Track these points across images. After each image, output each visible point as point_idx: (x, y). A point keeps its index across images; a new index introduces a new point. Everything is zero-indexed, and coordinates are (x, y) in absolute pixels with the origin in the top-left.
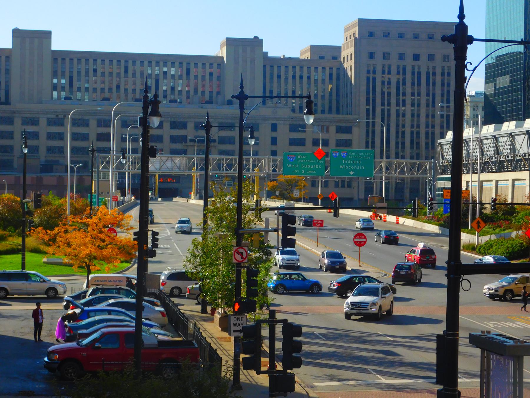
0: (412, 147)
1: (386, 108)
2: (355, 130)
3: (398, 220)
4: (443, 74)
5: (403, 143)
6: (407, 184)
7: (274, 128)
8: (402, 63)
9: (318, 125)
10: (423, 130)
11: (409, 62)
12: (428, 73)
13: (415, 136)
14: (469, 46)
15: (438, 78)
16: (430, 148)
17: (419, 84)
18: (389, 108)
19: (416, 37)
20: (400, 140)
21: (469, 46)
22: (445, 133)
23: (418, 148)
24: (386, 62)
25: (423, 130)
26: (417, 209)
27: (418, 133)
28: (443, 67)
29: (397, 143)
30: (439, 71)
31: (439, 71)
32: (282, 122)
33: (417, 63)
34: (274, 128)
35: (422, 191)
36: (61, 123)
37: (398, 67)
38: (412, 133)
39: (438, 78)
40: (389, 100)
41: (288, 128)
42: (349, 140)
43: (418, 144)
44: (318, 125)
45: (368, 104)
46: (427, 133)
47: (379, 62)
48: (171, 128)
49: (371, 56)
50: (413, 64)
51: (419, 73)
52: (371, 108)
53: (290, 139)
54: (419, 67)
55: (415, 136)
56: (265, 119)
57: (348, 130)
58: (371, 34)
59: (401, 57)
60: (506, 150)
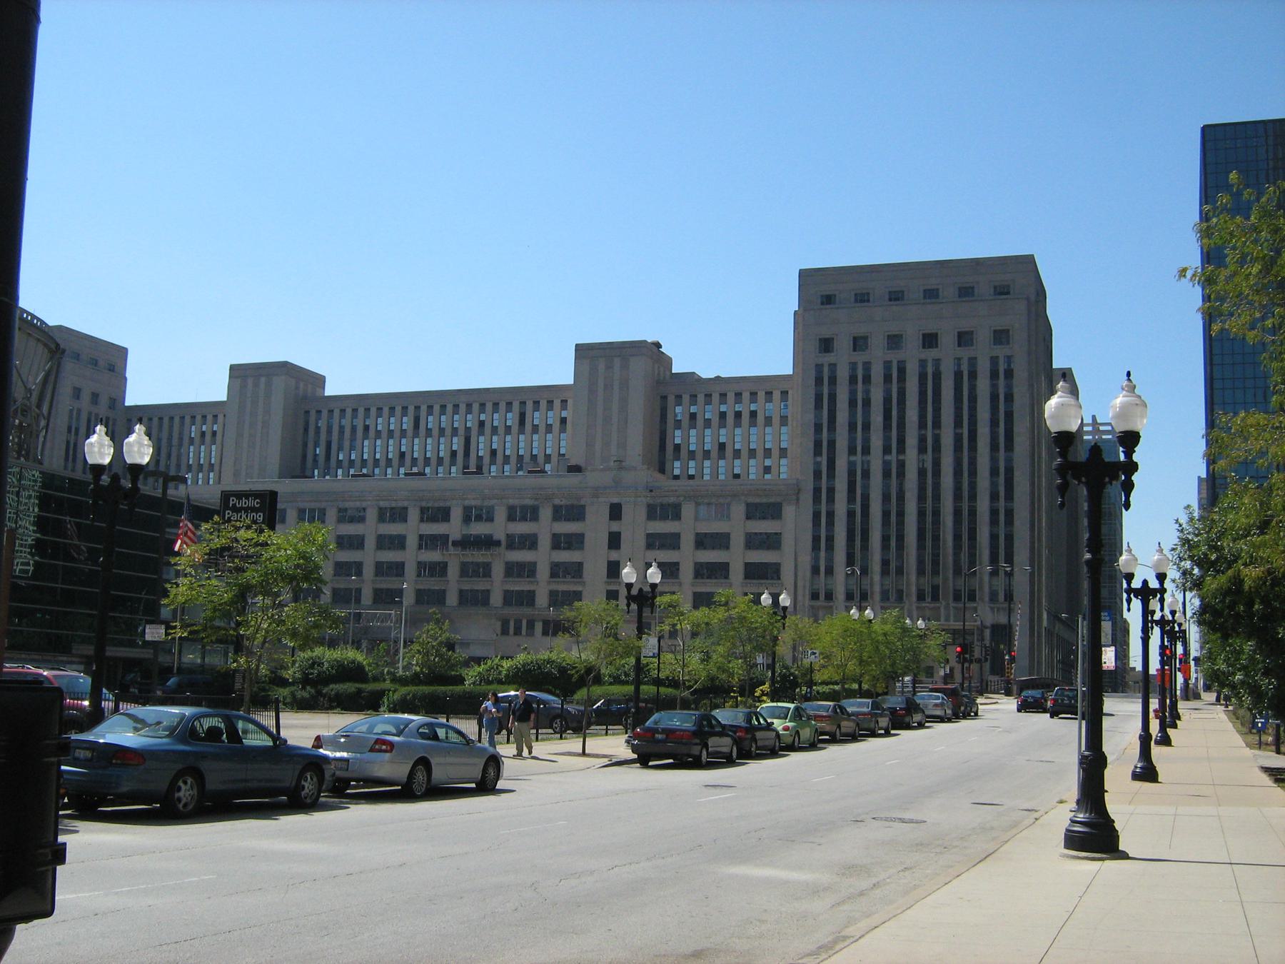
1: (893, 457)
2: (789, 511)
3: (165, 488)
4: (994, 375)
7: (616, 512)
8: (894, 357)
9: (709, 504)
11: (912, 354)
12: (958, 375)
14: (676, 369)
15: (983, 385)
17: (994, 398)
18: (853, 458)
19: (931, 294)
21: (676, 369)
24: (965, 353)
28: (959, 359)
30: (984, 367)
31: (984, 367)
33: (931, 354)
34: (616, 512)
36: (421, 596)
37: (887, 365)
39: (983, 385)
40: (866, 441)
41: (643, 512)
44: (709, 504)
47: (843, 357)
48: (422, 520)
50: (923, 357)
51: (937, 376)
54: (937, 362)
56: (597, 492)
57: (773, 511)
58: (828, 300)
59: (894, 341)
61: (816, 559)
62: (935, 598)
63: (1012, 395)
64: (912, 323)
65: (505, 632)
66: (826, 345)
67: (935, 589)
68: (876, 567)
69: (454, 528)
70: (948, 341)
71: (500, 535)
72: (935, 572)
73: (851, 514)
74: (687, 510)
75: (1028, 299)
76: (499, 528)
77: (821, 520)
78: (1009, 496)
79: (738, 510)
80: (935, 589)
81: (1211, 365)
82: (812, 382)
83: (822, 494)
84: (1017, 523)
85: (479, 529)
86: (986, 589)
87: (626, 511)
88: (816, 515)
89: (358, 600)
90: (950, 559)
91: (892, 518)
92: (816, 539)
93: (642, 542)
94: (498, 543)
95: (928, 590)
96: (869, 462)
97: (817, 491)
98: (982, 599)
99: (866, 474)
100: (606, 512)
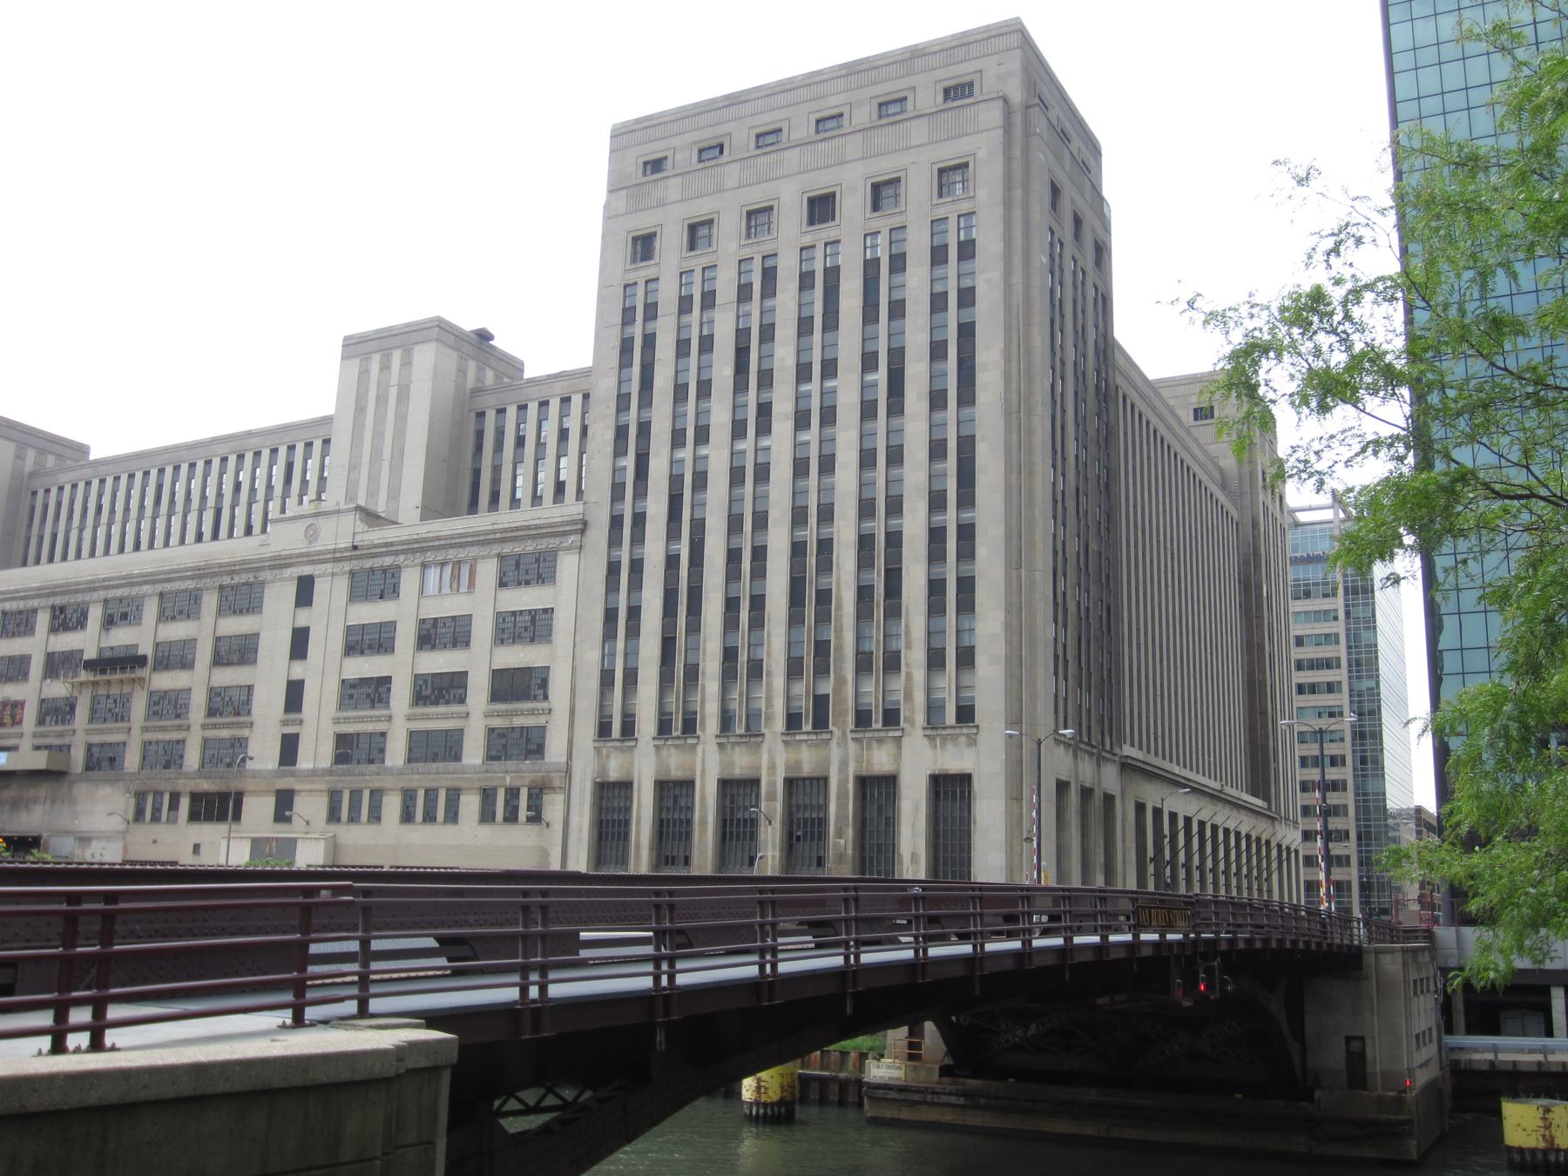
0: (795, 618)
2: (567, 565)
5: (758, 602)
6: (772, 797)
7: (305, 593)
10: (845, 531)
11: (790, 228)
12: (871, 267)
13: (812, 560)
16: (879, 613)
19: (827, 123)
20: (745, 589)
22: (1091, 163)
23: (823, 617)
25: (845, 531)
26: (366, 955)
27: (825, 546)
29: (731, 605)
32: (329, 567)
34: (305, 593)
35: (840, 834)
38: (798, 549)
42: (545, 611)
43: (824, 597)
45: (619, 450)
46: (865, 542)
49: (644, 246)
52: (629, 462)
53: (349, 630)
55: (812, 560)
56: (280, 563)
58: (656, 165)
60: (912, 855)
61: (607, 656)
62: (821, 722)
63: (707, 428)
64: (915, 157)
65: (139, 815)
66: (644, 246)
67: (821, 703)
68: (711, 666)
69: (87, 641)
70: (671, 245)
71: (146, 649)
72: (822, 670)
73: (672, 562)
74: (409, 580)
75: (1005, 100)
76: (140, 637)
77: (621, 575)
78: (967, 498)
79: (488, 571)
80: (821, 703)
81: (937, 794)
82: (617, 319)
83: (626, 527)
84: (981, 551)
85: (121, 637)
86: (920, 698)
87: (320, 589)
88: (613, 569)
89: (95, 700)
90: (849, 638)
91: (746, 562)
92: (610, 615)
93: (338, 644)
94: (141, 661)
95: (805, 705)
96: (834, 391)
97: (616, 522)
98: (910, 720)
99: (701, 481)
100: (291, 590)
